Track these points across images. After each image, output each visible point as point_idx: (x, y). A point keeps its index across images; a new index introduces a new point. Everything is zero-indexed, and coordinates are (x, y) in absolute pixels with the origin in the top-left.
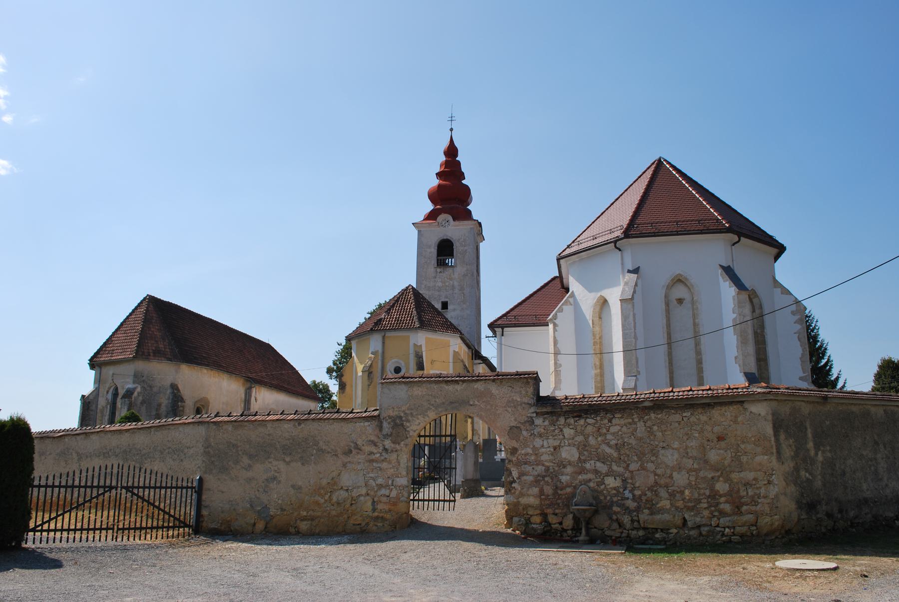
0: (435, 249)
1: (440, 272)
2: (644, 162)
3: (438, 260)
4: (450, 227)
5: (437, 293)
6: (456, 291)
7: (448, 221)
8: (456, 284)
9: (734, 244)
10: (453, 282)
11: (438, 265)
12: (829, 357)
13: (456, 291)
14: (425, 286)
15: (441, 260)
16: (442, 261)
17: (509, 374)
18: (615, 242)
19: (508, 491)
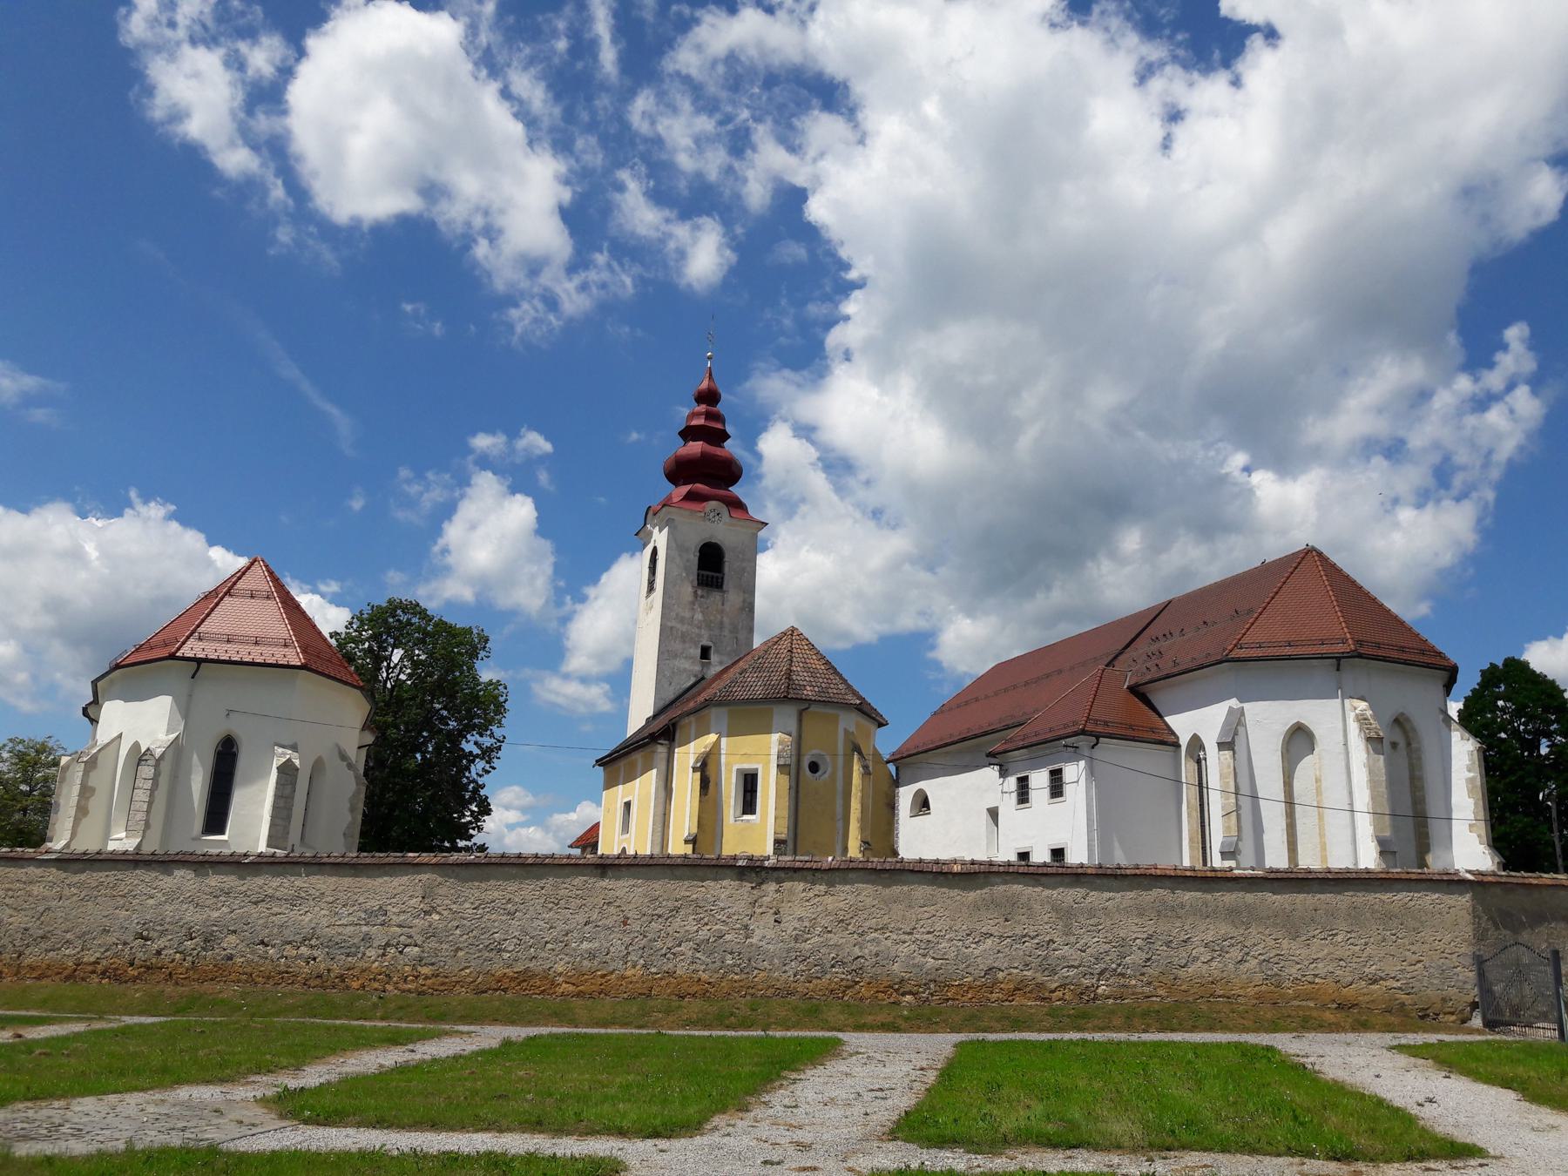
0: (695, 556)
1: (702, 597)
2: (985, 811)
3: (698, 575)
4: (721, 524)
5: (697, 631)
6: (726, 633)
7: (718, 514)
8: (726, 620)
9: (1093, 747)
10: (722, 617)
11: (698, 584)
12: (655, 541)
13: (726, 633)
14: (677, 615)
15: (703, 575)
16: (715, 580)
17: (280, 869)
18: (1338, 659)
19: (595, 1021)
